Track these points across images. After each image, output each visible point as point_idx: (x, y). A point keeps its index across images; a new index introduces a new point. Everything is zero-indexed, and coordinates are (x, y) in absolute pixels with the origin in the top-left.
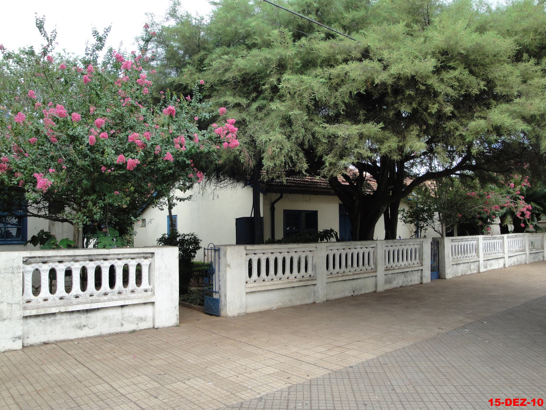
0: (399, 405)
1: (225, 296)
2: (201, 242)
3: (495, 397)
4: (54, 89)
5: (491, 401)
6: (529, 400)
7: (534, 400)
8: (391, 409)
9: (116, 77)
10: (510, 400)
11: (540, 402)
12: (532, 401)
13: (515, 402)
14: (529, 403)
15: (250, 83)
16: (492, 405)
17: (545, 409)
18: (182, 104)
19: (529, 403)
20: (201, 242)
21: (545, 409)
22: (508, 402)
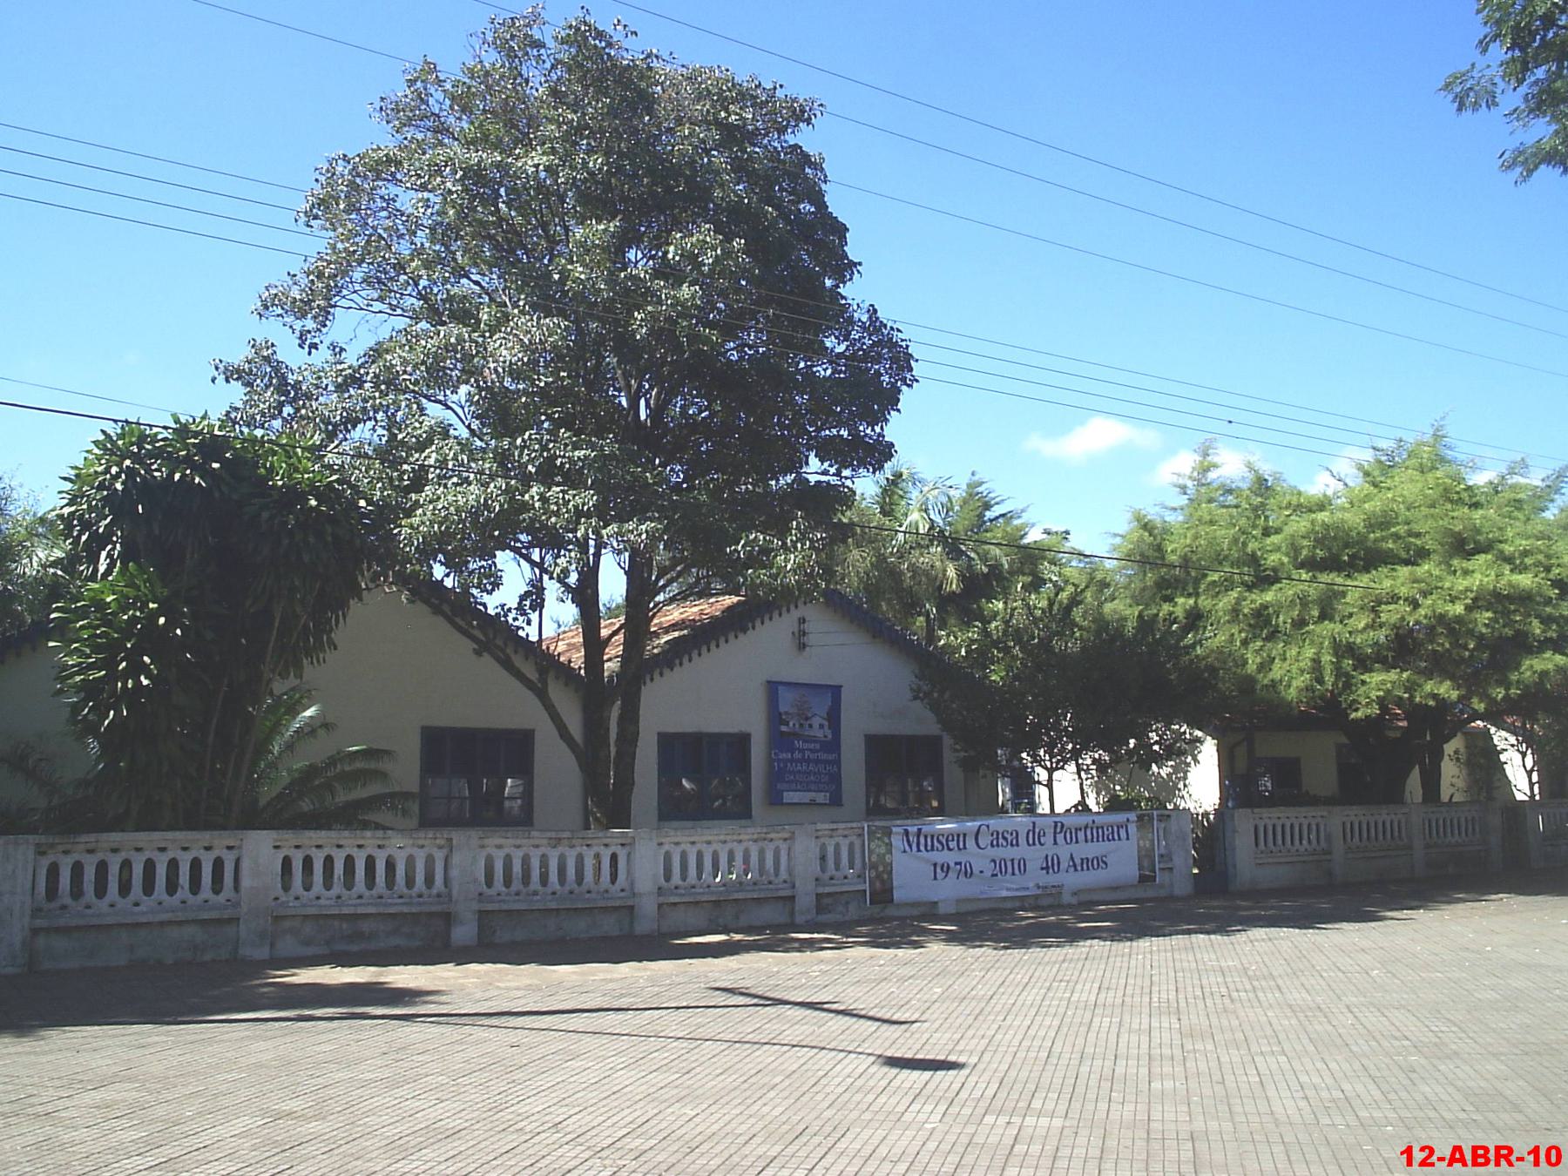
0: (1333, 1169)
1: (1235, 866)
2: (503, 574)
3: (1419, 1139)
4: (1314, 508)
5: (1408, 1151)
6: (1521, 1147)
7: (1535, 1151)
8: (1150, 1174)
9: (477, 137)
10: (1486, 1149)
11: (1554, 1156)
12: (1529, 1153)
13: (1480, 1156)
14: (1520, 1159)
15: (605, 168)
16: (1410, 1163)
17: (1245, 1175)
18: (1359, 524)
19: (1520, 1159)
20: (503, 574)
21: (1245, 1175)
22: (1456, 1156)
